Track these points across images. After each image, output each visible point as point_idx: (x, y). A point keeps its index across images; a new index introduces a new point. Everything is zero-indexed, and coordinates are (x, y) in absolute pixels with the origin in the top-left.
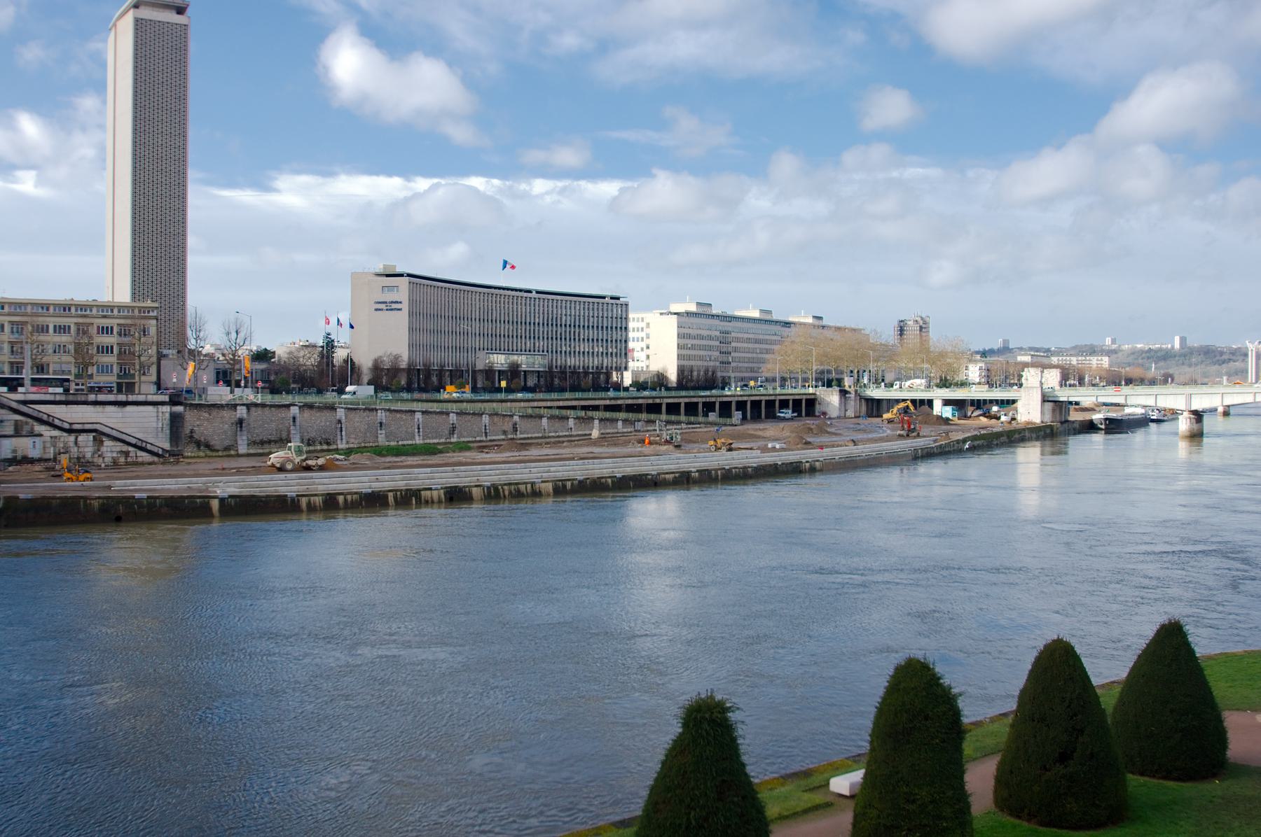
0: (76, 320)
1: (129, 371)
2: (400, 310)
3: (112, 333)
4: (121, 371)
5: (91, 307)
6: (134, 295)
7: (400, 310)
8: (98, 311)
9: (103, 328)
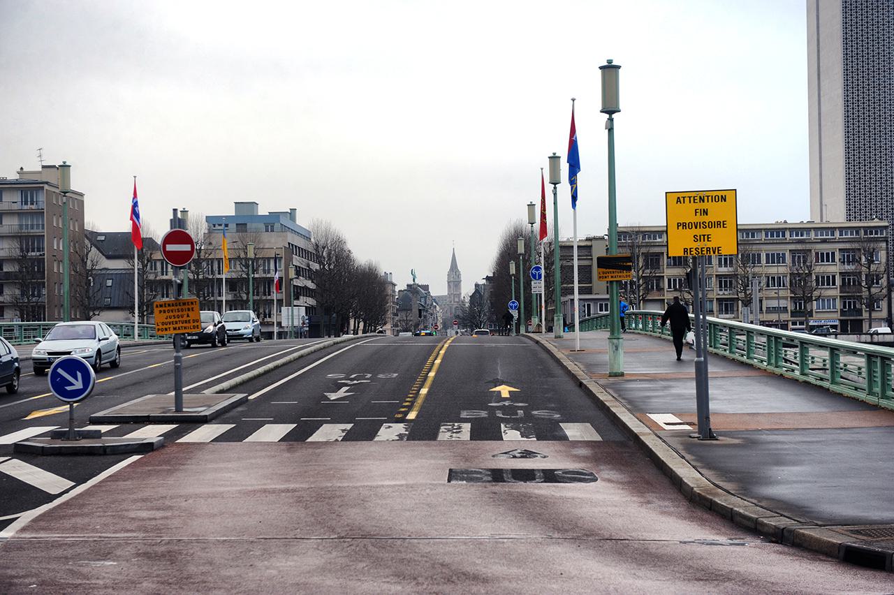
0: (793, 247)
1: (855, 306)
2: (690, 202)
3: (833, 260)
4: (845, 307)
5: (783, 231)
6: (853, 210)
7: (690, 202)
8: (816, 235)
9: (822, 254)
